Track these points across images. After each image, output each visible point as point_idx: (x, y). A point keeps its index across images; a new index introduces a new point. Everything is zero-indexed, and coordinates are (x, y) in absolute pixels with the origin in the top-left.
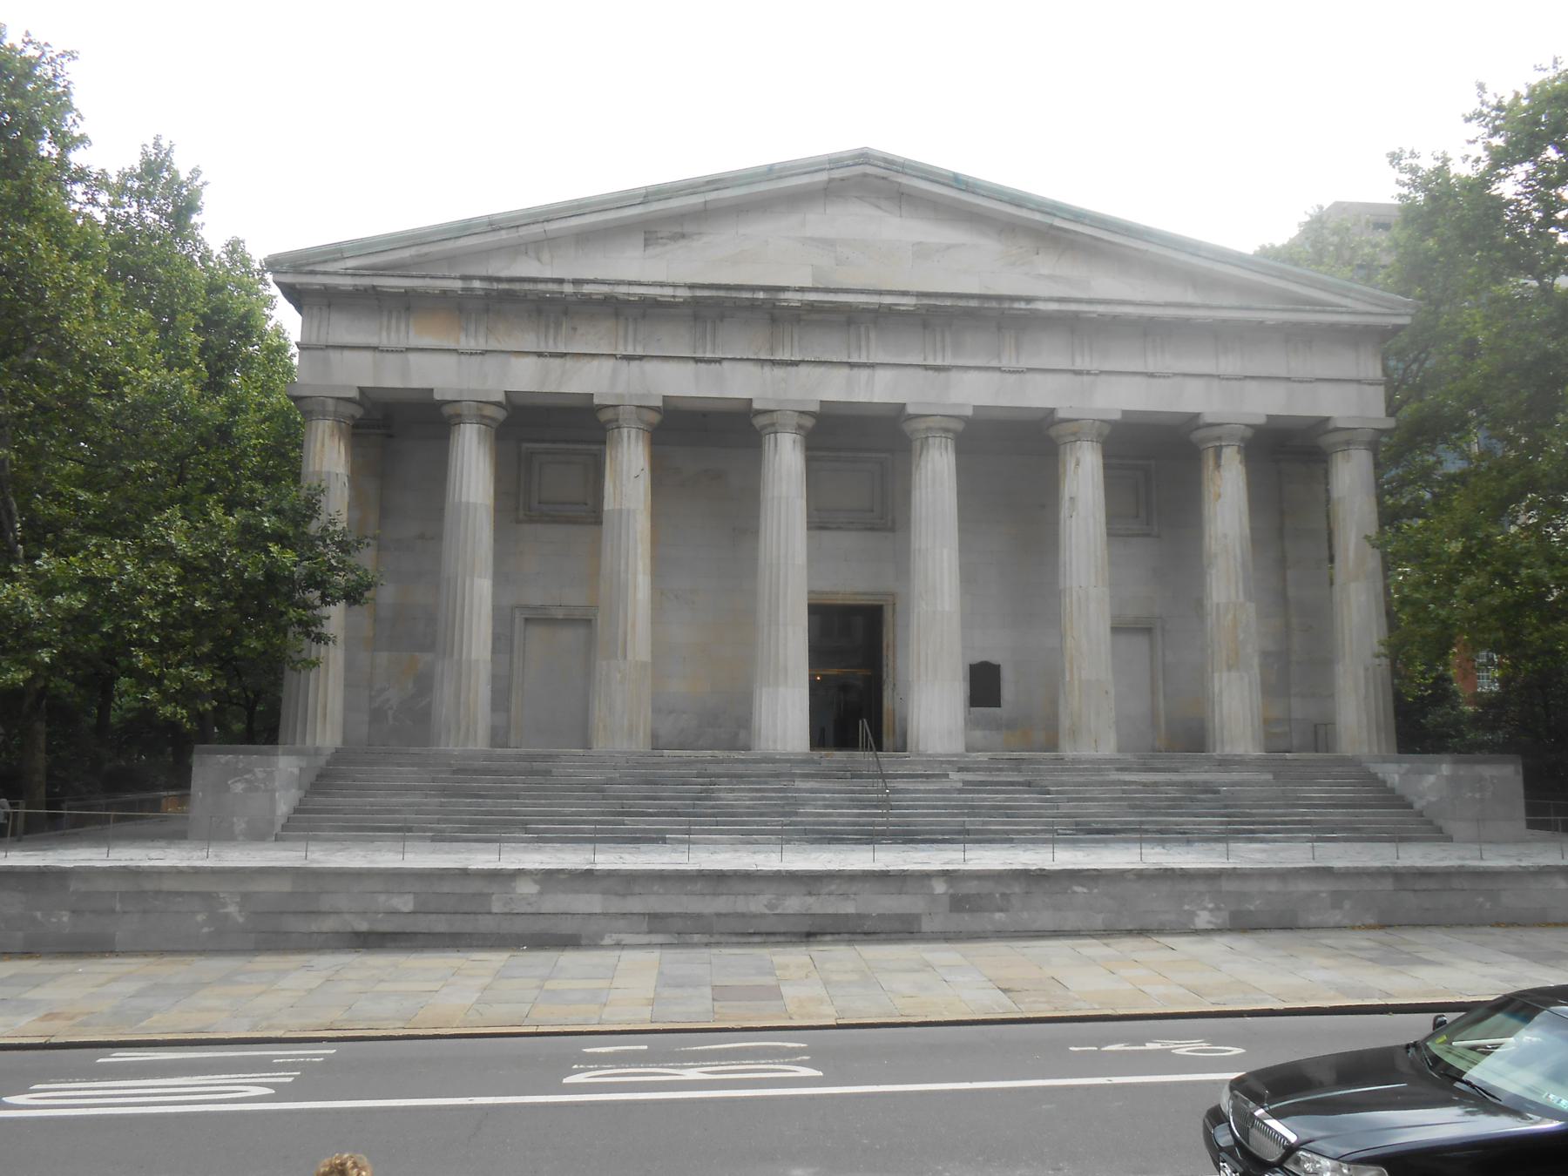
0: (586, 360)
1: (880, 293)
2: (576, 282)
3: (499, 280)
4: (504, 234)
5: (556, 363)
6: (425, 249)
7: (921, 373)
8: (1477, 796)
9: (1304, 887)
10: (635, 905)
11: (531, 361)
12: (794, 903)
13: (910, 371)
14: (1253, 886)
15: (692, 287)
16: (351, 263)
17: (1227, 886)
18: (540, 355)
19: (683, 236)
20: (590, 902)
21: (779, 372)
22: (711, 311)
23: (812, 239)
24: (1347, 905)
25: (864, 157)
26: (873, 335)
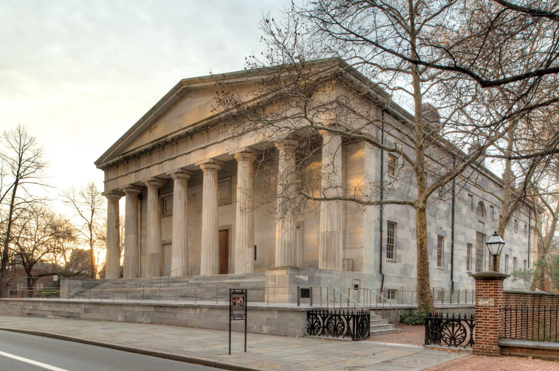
1: (185, 128)
4: (124, 141)
5: (137, 173)
6: (114, 150)
7: (200, 150)
8: (273, 283)
9: (137, 309)
10: (51, 309)
11: (133, 174)
12: (68, 309)
13: (198, 151)
14: (128, 309)
15: (152, 142)
16: (105, 159)
17: (124, 308)
18: (135, 172)
19: (156, 127)
20: (46, 308)
21: (172, 162)
22: (161, 146)
23: (178, 116)
24: (145, 315)
25: (181, 84)
26: (191, 142)
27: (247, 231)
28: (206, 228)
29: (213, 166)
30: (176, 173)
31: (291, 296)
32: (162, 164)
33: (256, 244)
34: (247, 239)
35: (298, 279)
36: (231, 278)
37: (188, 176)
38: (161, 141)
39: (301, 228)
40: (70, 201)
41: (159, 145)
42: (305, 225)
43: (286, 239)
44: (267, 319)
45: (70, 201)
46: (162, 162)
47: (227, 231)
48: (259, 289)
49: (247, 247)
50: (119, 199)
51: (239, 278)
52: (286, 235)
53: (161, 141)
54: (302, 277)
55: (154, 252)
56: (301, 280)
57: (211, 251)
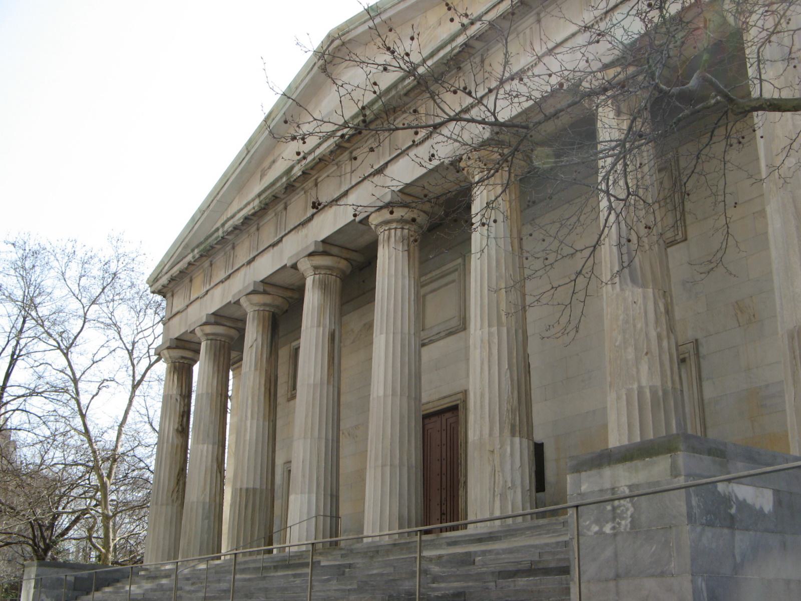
0: (236, 273)
2: (223, 225)
3: (201, 243)
5: (227, 283)
8: (608, 529)
25: (331, 38)
27: (506, 377)
28: (381, 393)
29: (399, 213)
30: (311, 255)
31: (701, 583)
32: (280, 245)
33: (538, 437)
34: (505, 407)
35: (727, 500)
36: (454, 543)
37: (343, 264)
38: (279, 184)
39: (692, 362)
40: (108, 396)
41: (275, 198)
42: (703, 350)
43: (644, 382)
44: (76, 578)
45: (108, 396)
46: (280, 240)
47: (454, 409)
48: (547, 572)
49: (507, 432)
50: (193, 366)
51: (480, 540)
52: (644, 368)
53: (279, 184)
54: (744, 492)
55: (251, 486)
56: (743, 505)
57: (397, 462)
